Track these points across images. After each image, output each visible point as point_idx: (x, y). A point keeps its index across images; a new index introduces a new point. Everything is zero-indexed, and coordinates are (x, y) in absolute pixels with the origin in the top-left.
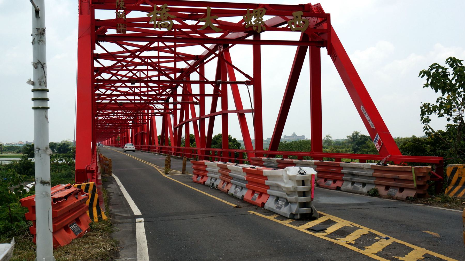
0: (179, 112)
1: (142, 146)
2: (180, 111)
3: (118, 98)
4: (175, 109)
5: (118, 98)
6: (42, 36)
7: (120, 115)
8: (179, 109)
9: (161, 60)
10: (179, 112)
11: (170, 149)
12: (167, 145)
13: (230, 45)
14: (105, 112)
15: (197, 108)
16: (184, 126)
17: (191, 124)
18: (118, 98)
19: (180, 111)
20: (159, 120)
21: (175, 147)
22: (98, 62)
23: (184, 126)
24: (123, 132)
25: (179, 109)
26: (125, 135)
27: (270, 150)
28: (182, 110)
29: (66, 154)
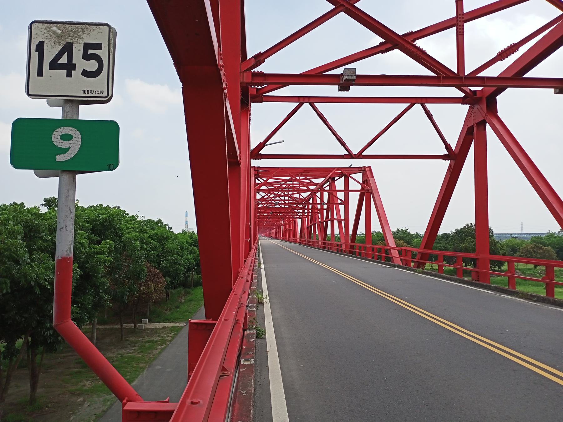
0: (325, 211)
1: (300, 239)
2: (326, 210)
3: (275, 199)
4: (322, 209)
5: (275, 199)
6: (260, 306)
7: (283, 206)
8: (325, 209)
9: (294, 186)
10: (325, 211)
11: (305, 241)
12: (304, 239)
13: (336, 178)
14: (288, 178)
15: (342, 208)
16: (329, 222)
17: (336, 222)
18: (275, 199)
19: (326, 210)
20: (299, 221)
21: (322, 241)
22: (259, 180)
23: (329, 222)
24: (277, 228)
25: (325, 209)
26: (278, 230)
27: (424, 249)
28: (328, 210)
29: (9, 287)
